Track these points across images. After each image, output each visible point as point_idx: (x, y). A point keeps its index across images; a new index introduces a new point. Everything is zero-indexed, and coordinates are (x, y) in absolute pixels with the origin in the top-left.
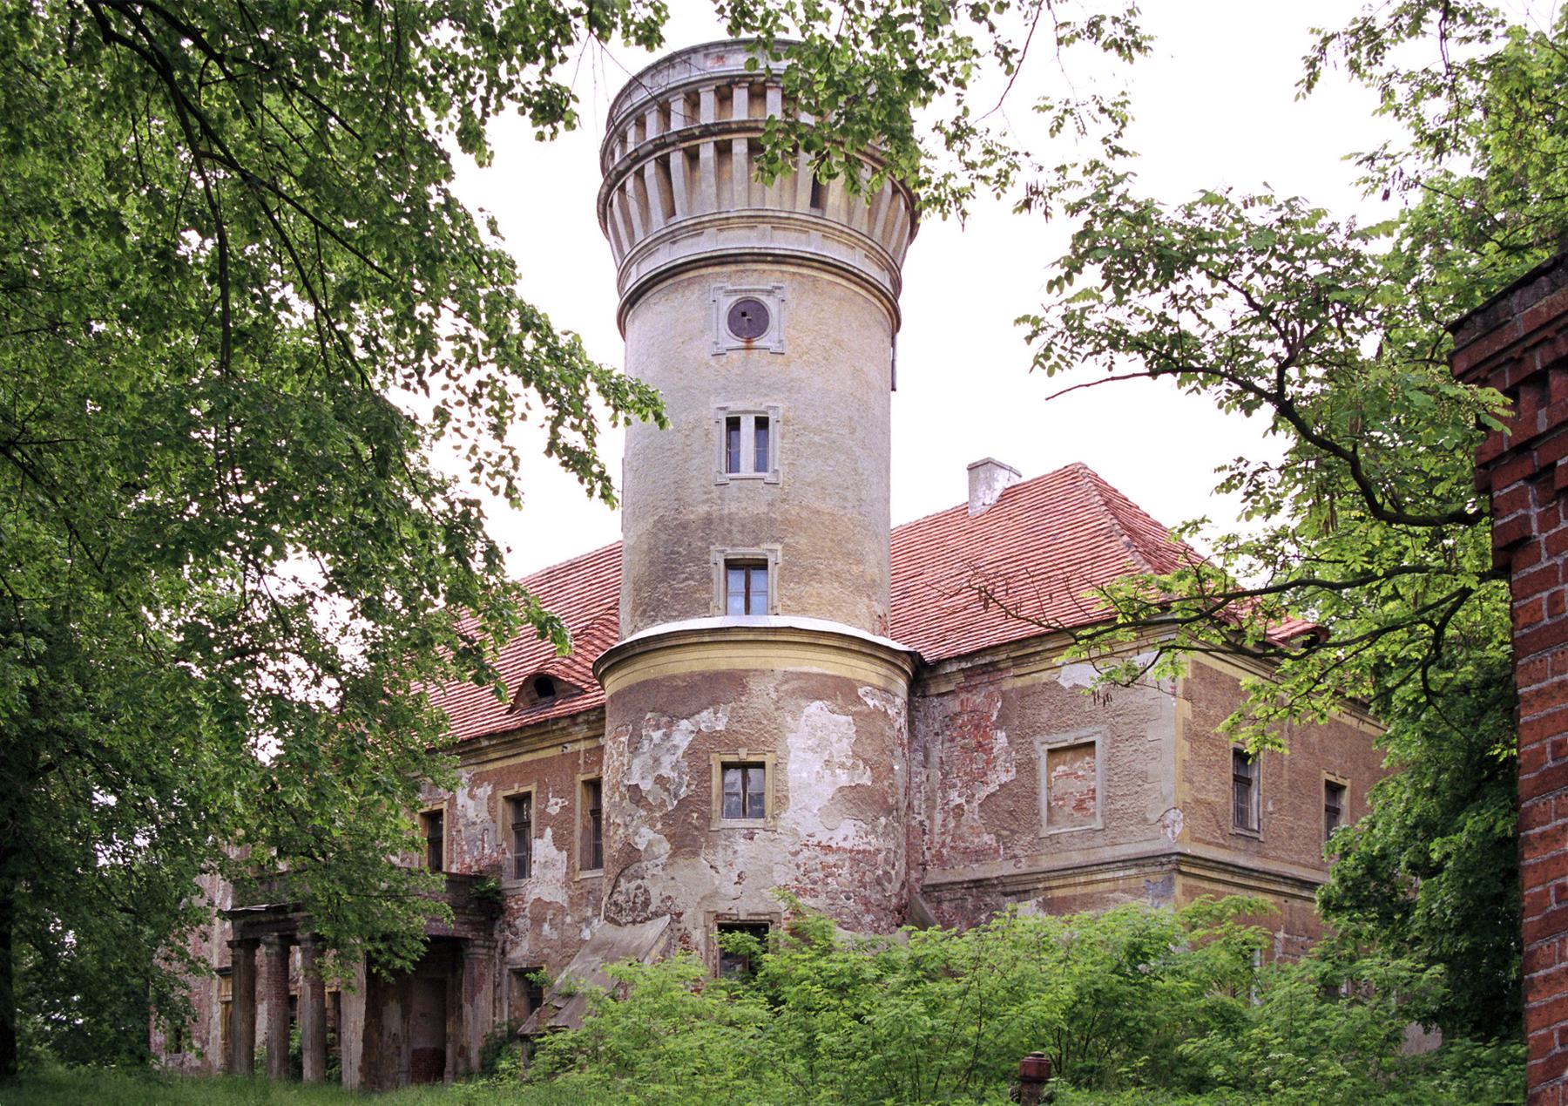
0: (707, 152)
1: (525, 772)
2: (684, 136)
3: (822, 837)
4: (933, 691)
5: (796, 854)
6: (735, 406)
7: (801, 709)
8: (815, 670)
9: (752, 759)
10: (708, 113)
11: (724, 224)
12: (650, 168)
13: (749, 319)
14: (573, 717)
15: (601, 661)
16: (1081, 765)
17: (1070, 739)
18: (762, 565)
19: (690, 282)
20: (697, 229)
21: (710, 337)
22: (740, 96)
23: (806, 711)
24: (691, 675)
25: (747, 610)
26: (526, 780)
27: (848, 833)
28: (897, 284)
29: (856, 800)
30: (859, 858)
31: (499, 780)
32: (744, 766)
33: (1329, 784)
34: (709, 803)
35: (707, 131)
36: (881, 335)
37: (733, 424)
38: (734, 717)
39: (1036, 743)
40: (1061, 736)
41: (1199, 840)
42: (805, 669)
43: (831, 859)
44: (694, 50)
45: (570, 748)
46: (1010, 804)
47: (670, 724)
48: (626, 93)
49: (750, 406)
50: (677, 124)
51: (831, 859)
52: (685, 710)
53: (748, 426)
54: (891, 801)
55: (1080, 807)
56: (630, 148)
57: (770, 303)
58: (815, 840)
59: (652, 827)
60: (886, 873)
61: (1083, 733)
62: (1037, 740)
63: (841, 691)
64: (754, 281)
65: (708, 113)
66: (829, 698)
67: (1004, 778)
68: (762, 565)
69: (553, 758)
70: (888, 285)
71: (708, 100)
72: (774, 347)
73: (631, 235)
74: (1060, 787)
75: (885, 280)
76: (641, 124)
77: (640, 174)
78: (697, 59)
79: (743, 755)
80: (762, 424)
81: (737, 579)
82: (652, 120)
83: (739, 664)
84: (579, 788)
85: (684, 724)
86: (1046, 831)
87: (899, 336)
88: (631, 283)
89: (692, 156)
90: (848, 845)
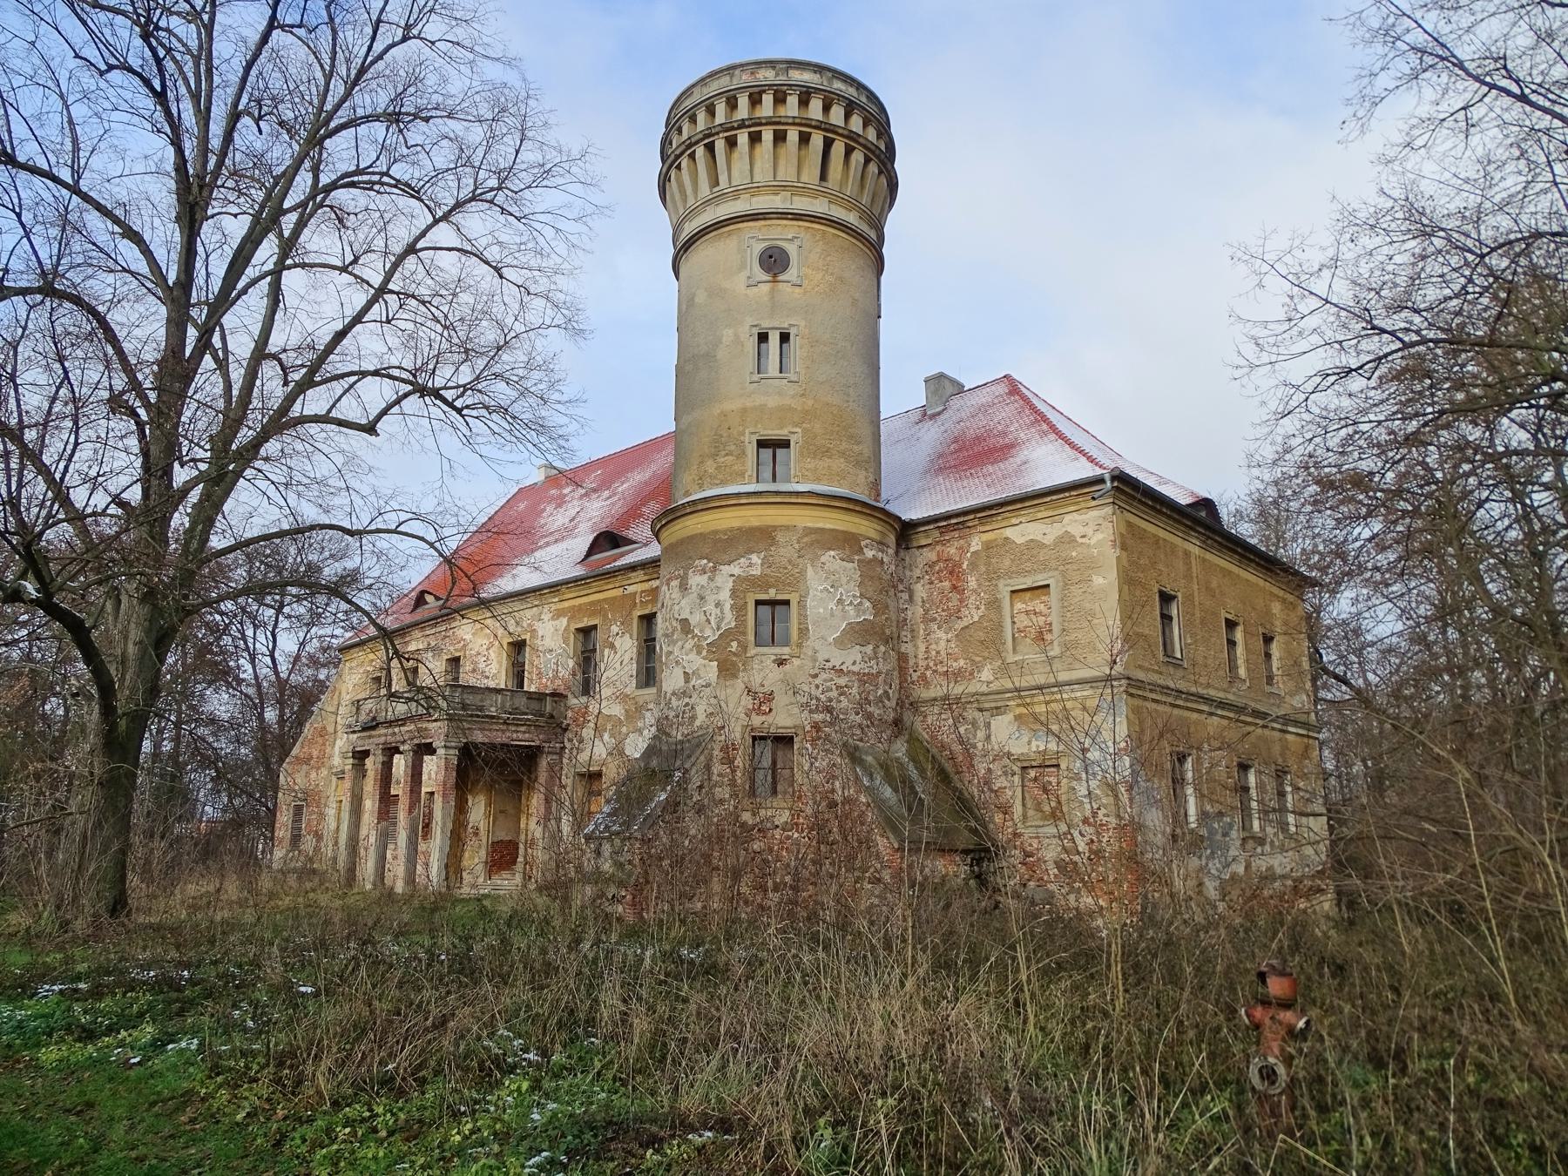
0: (743, 138)
1: (595, 609)
2: (725, 128)
3: (836, 662)
4: (915, 544)
5: (816, 676)
7: (818, 557)
8: (828, 526)
9: (779, 597)
10: (743, 111)
11: (754, 190)
12: (700, 151)
13: (774, 261)
15: (658, 519)
17: (1029, 582)
18: (786, 444)
19: (730, 233)
20: (736, 194)
21: (746, 273)
22: (768, 99)
23: (823, 559)
24: (731, 530)
25: (774, 480)
26: (593, 614)
27: (852, 658)
29: (860, 634)
30: (864, 679)
31: (574, 613)
32: (773, 603)
33: (1227, 620)
34: (744, 634)
35: (742, 125)
36: (871, 275)
37: (763, 338)
39: (1001, 586)
40: (1022, 580)
41: (1140, 667)
42: (820, 525)
43: (842, 681)
44: (693, 86)
45: (631, 589)
48: (687, 93)
50: (720, 118)
51: (842, 681)
52: (726, 558)
53: (774, 339)
54: (888, 632)
56: (685, 135)
57: (791, 249)
58: (829, 665)
59: (699, 653)
60: (886, 692)
61: (1040, 577)
62: (1001, 584)
63: (848, 543)
64: (783, 234)
65: (743, 111)
66: (838, 548)
68: (786, 444)
69: (614, 598)
71: (743, 101)
72: (794, 279)
73: (685, 201)
74: (1022, 621)
75: (873, 235)
76: (693, 120)
77: (692, 156)
78: (696, 90)
79: (772, 594)
81: (767, 454)
82: (701, 116)
83: (769, 521)
84: (635, 621)
85: (725, 569)
86: (1011, 658)
87: (883, 278)
88: (684, 236)
90: (856, 668)
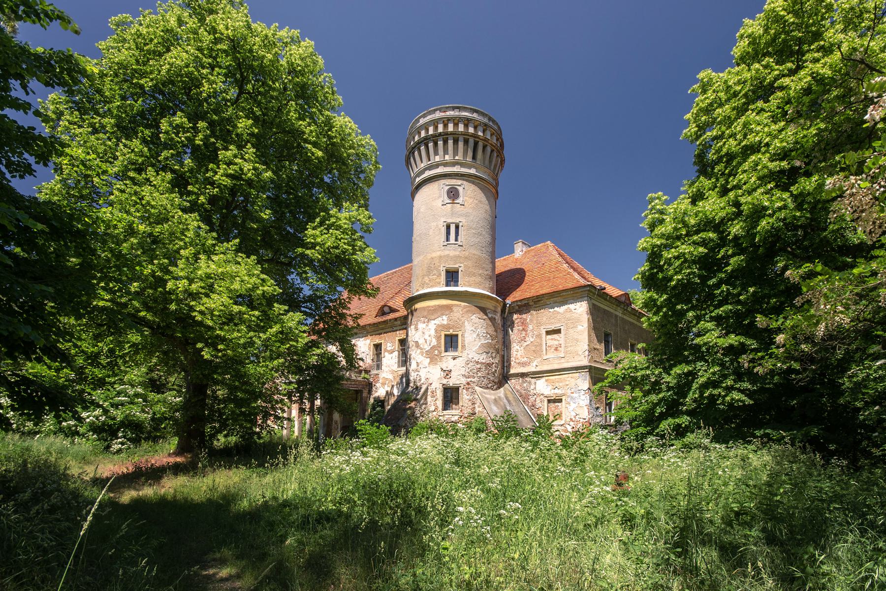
2: (433, 136)
6: (449, 221)
14: (396, 319)
16: (555, 336)
17: (552, 327)
28: (497, 184)
35: (440, 134)
37: (448, 227)
38: (449, 320)
46: (534, 348)
47: (428, 322)
49: (453, 221)
52: (433, 317)
55: (556, 349)
57: (460, 189)
62: (542, 327)
65: (441, 129)
67: (532, 340)
70: (491, 180)
72: (461, 202)
80: (457, 227)
84: (397, 342)
89: (436, 144)
